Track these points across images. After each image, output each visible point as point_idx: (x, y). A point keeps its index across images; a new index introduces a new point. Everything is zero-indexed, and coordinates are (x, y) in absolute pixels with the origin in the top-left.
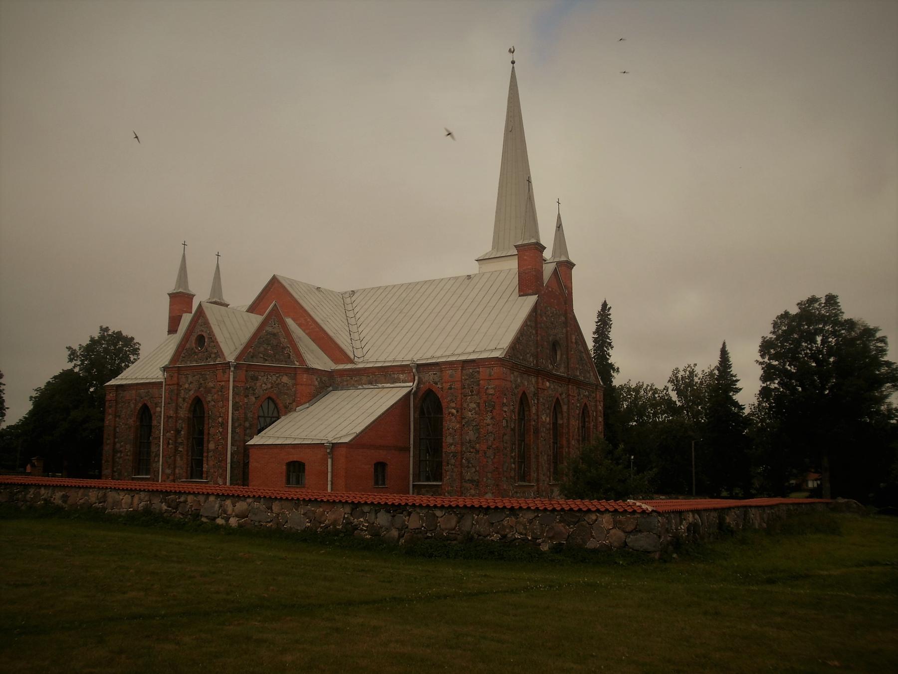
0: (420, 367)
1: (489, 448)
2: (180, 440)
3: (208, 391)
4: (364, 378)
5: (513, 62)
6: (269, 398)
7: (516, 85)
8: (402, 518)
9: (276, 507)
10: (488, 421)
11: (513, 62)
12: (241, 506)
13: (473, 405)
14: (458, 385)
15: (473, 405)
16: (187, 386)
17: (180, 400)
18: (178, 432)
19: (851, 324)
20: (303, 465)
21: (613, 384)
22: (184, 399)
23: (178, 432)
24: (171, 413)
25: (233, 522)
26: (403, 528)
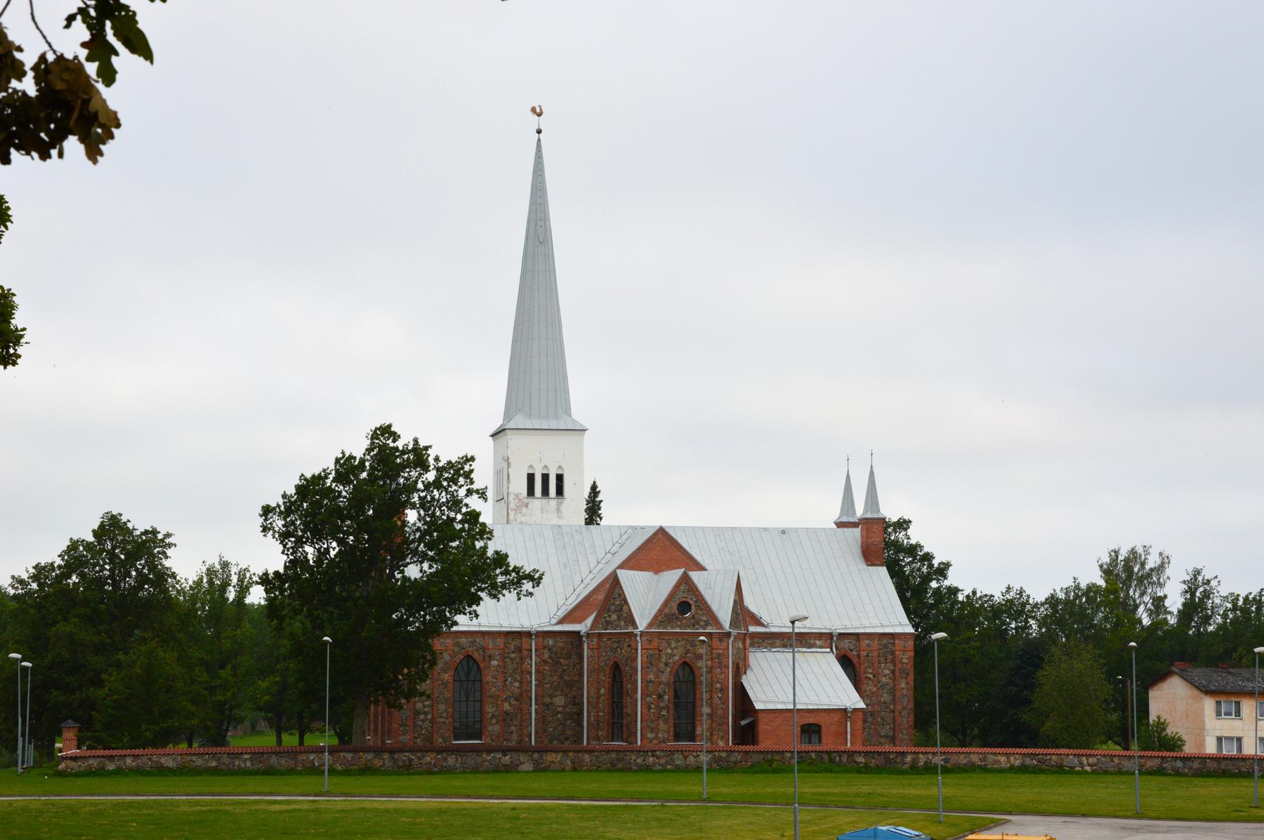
0: (842, 636)
1: (904, 708)
2: (662, 705)
3: (700, 657)
4: (778, 642)
5: (539, 132)
6: (685, 663)
7: (543, 182)
8: (1189, 764)
9: (1116, 760)
10: (903, 685)
11: (539, 132)
12: (1092, 760)
13: (887, 672)
14: (875, 654)
15: (887, 672)
16: (669, 651)
17: (662, 665)
18: (660, 696)
19: (1052, 601)
20: (820, 726)
21: (263, 602)
22: (666, 664)
23: (660, 696)
24: (651, 677)
25: (1088, 768)
26: (1190, 768)
